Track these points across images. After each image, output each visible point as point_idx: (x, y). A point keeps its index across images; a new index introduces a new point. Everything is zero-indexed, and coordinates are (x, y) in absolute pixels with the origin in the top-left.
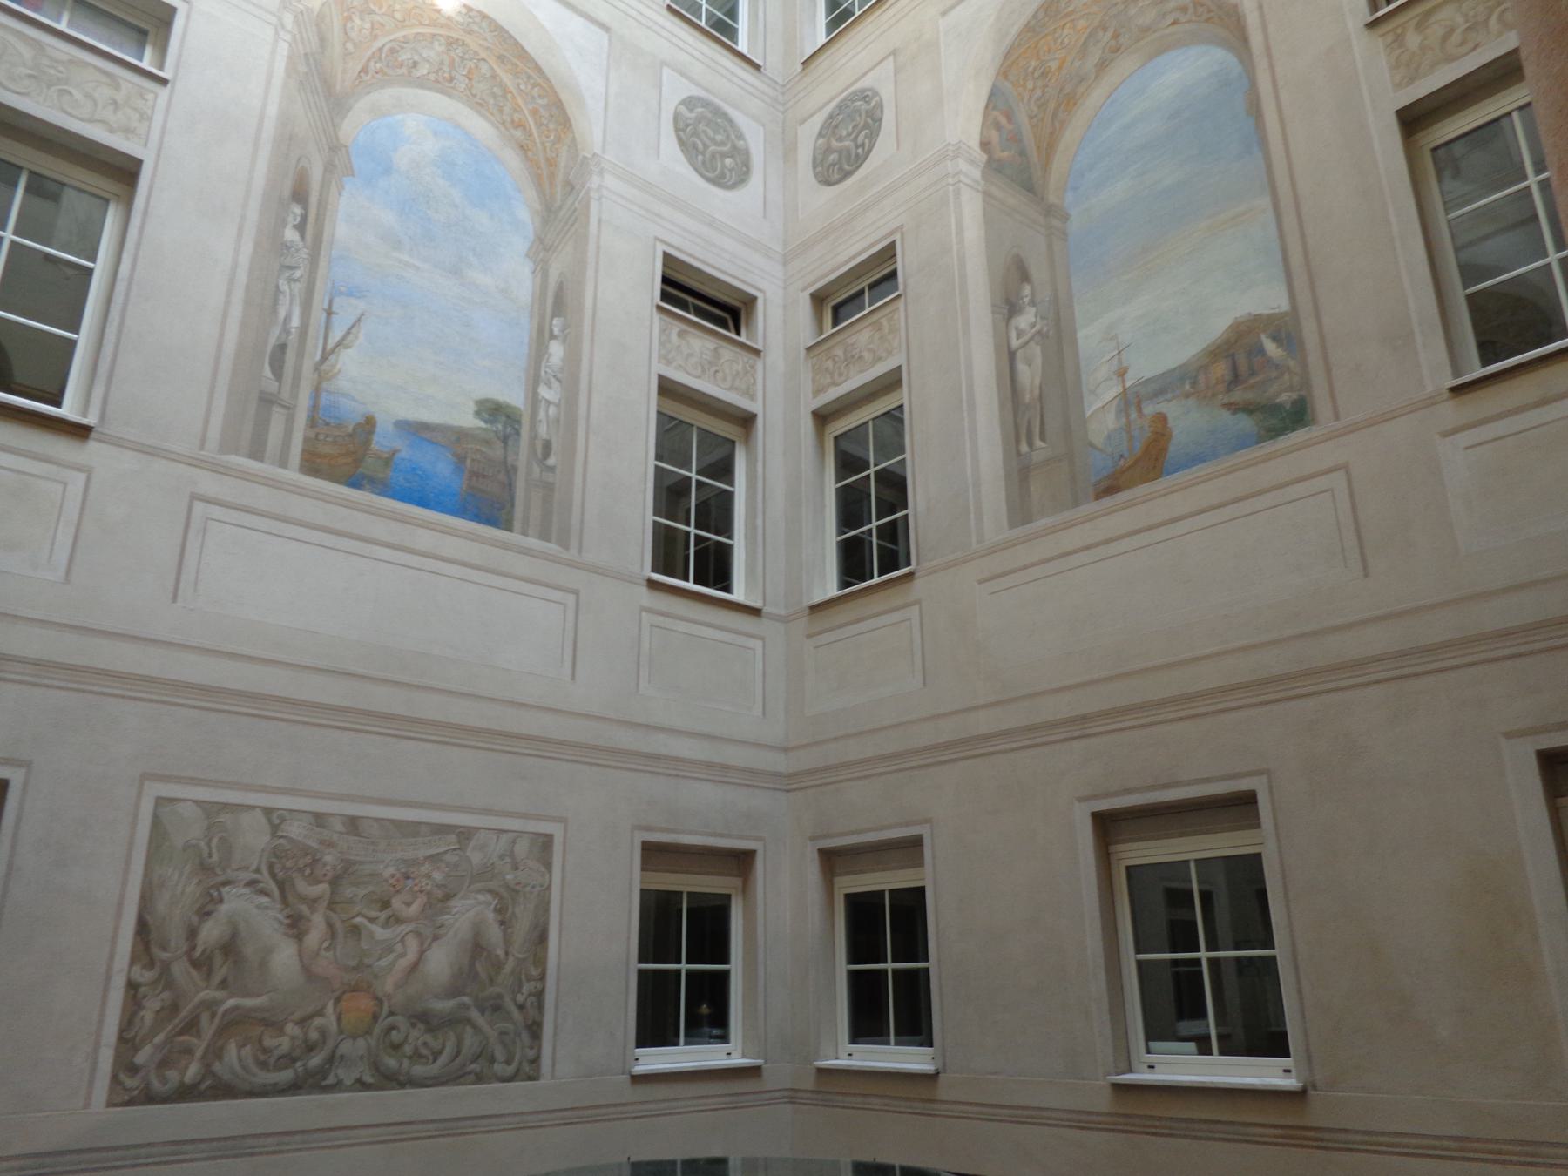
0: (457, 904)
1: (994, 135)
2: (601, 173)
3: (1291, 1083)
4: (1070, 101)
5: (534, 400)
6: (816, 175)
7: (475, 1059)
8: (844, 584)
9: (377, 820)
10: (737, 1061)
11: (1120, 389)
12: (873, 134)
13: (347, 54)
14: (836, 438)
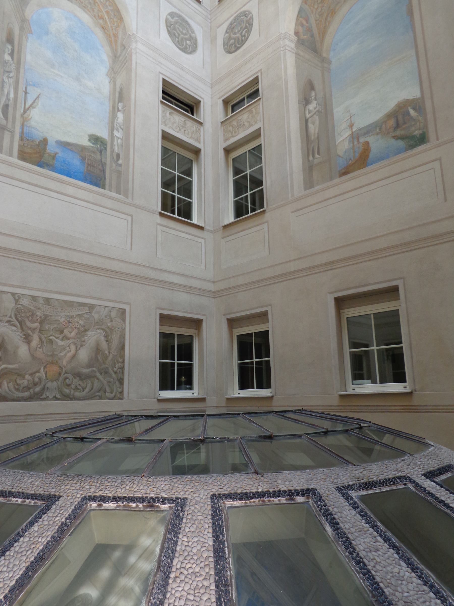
0: (89, 333)
1: (301, 29)
2: (136, 42)
3: (408, 390)
4: (102, 161)
5: (112, 136)
6: (224, 49)
7: (99, 391)
9: (57, 300)
10: (196, 395)
11: (351, 133)
12: (249, 31)
14: (233, 159)
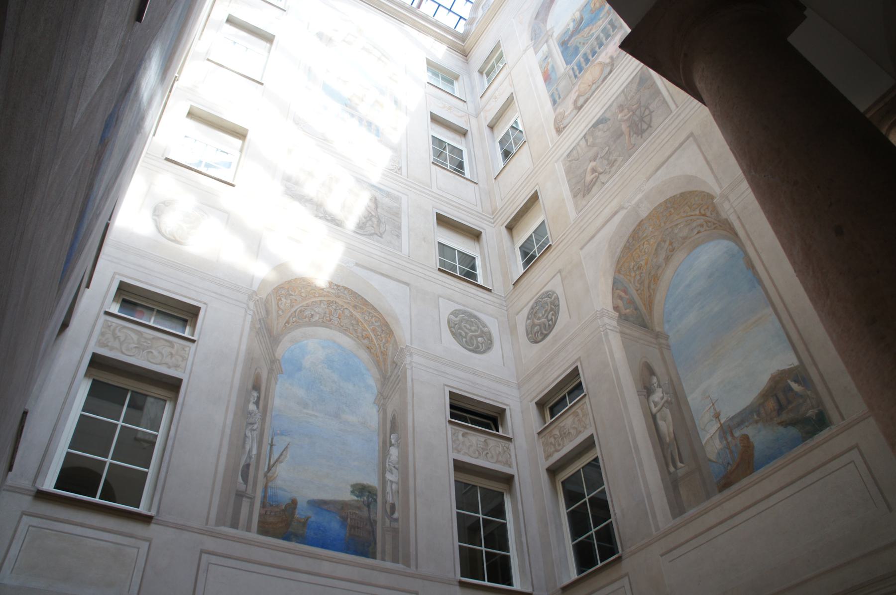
1: (620, 303)
2: (411, 355)
4: (655, 279)
5: (384, 481)
8: (580, 571)
13: (279, 316)
14: (563, 483)
